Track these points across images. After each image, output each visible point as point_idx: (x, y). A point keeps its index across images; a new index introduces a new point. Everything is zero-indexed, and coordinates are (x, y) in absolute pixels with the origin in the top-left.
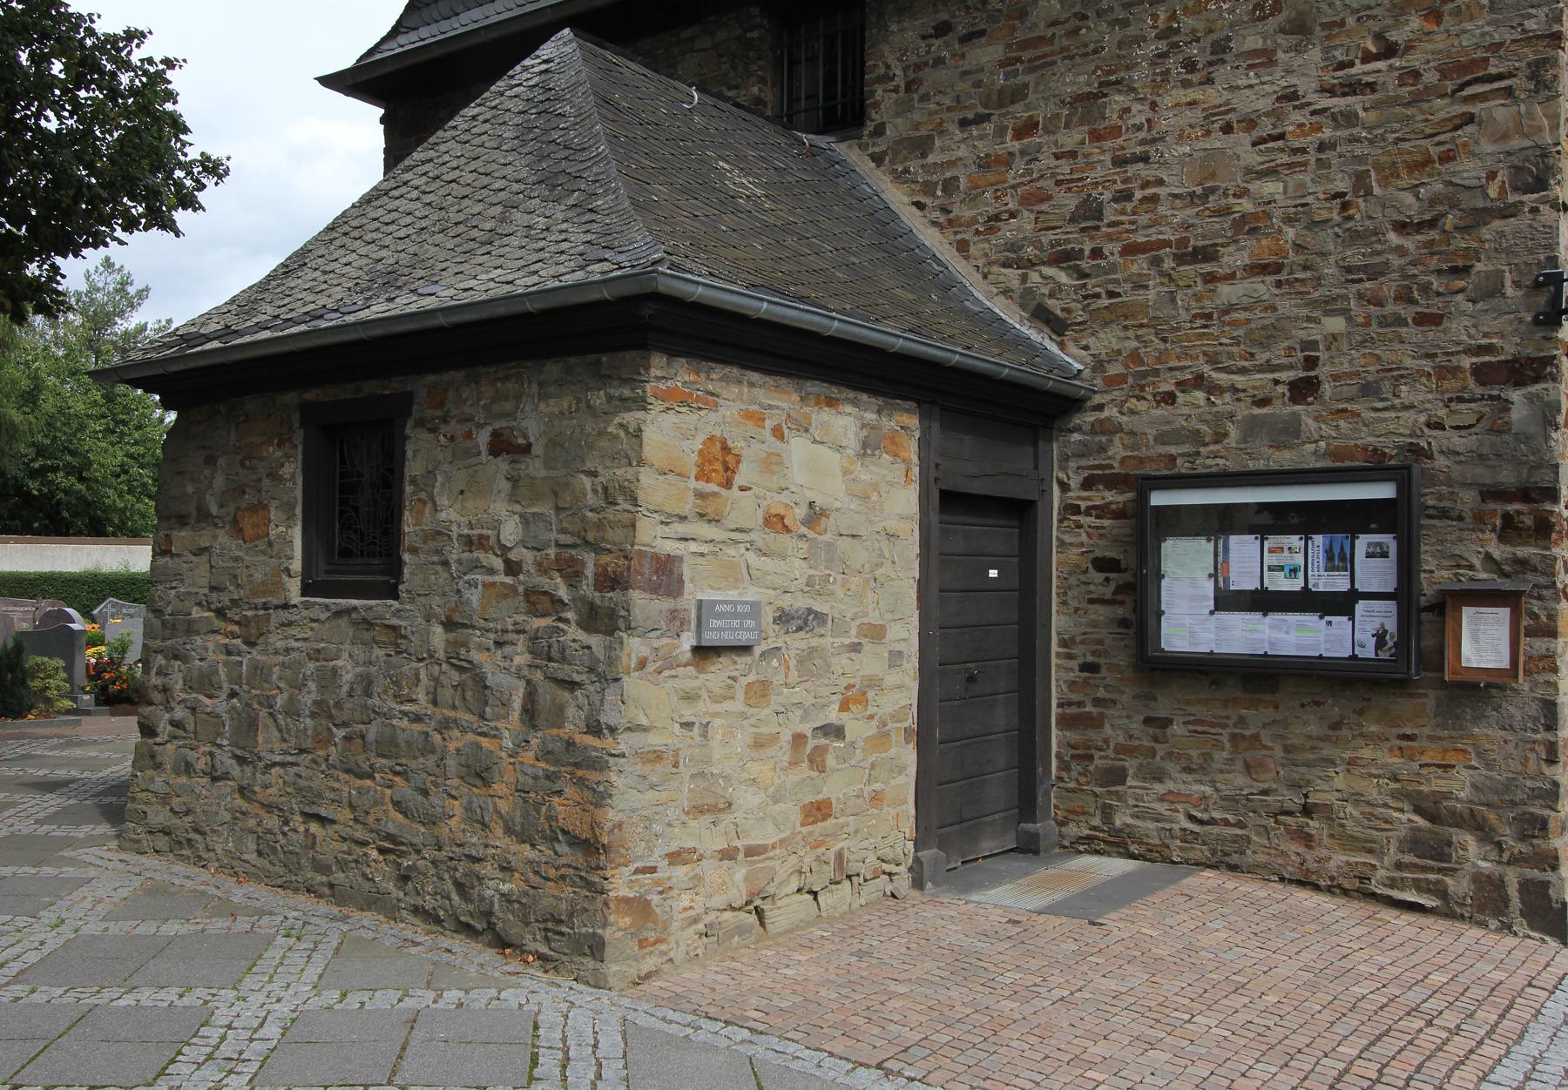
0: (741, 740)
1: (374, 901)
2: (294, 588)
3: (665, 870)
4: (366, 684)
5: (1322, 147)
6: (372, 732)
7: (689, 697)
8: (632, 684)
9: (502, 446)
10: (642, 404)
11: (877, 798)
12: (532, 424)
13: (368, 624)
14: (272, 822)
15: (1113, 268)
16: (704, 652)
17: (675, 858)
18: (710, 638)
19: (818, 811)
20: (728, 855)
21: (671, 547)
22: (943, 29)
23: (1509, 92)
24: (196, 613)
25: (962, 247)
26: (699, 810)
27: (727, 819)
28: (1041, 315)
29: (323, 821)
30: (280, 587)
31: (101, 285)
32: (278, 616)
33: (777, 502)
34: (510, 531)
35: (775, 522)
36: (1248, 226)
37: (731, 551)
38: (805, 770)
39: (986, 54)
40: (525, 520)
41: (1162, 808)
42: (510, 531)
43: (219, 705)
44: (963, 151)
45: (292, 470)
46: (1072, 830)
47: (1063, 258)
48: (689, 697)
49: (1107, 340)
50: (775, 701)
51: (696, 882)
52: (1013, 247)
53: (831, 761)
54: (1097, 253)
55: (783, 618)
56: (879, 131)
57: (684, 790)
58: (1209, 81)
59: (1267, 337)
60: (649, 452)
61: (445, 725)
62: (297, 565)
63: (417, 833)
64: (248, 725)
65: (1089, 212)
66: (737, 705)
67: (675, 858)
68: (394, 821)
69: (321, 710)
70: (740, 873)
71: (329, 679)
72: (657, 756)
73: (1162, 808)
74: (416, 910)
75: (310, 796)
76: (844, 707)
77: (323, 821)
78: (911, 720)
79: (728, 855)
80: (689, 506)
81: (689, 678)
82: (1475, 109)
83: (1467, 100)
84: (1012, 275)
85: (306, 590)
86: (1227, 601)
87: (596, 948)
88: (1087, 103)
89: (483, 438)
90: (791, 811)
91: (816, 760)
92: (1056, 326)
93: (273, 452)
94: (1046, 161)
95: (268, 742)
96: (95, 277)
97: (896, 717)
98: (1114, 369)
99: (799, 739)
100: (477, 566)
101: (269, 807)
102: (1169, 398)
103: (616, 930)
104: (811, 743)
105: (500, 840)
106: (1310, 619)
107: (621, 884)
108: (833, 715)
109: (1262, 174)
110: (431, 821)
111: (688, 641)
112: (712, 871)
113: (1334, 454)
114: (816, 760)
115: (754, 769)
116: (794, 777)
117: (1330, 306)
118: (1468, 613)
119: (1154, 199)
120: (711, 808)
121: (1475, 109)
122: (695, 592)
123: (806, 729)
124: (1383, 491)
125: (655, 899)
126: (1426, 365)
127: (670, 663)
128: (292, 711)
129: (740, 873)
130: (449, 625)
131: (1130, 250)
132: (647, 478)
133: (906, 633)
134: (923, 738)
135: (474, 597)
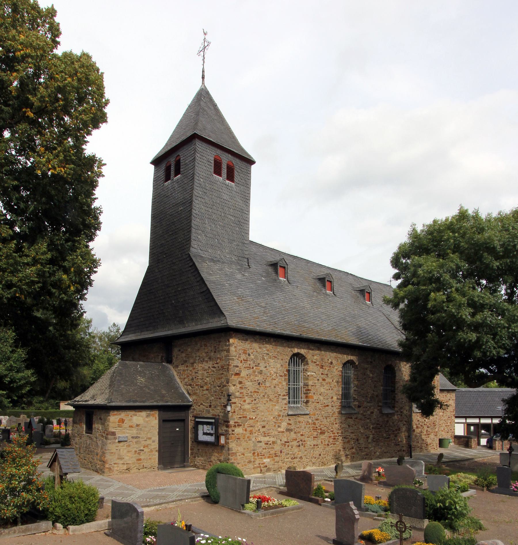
0: (125, 451)
1: (89, 469)
2: (84, 433)
3: (113, 465)
4: (89, 444)
5: (212, 375)
6: (90, 450)
7: (117, 446)
8: (109, 445)
9: (100, 419)
10: (110, 416)
11: (150, 459)
12: (102, 417)
13: (90, 437)
14: (81, 460)
15: (195, 387)
16: (119, 442)
17: (115, 464)
18: (120, 440)
19: (140, 460)
20: (123, 464)
21: (114, 431)
22: (180, 350)
23: (225, 371)
24: (76, 435)
25: (181, 382)
26: (119, 459)
27: (124, 460)
28: (188, 393)
29: (86, 460)
30: (82, 432)
31: (112, 330)
32: (83, 436)
33: (131, 424)
34: (100, 428)
35: (131, 427)
36: (206, 383)
37: (124, 430)
38: (137, 455)
39: (184, 355)
40: (102, 427)
41: (199, 461)
42: (100, 428)
43: (77, 446)
44: (181, 368)
45: (84, 418)
46: (192, 464)
47: (190, 385)
48: (117, 446)
49: (194, 397)
50: (131, 447)
51: (118, 467)
52: (186, 383)
53: (141, 454)
54: (193, 385)
55: (133, 437)
56: (173, 364)
57: (117, 456)
58: (203, 364)
59: (207, 399)
60: (111, 421)
61: (95, 449)
62: (85, 430)
63: (93, 461)
64: (80, 449)
65: (193, 379)
66: (125, 447)
67: (115, 464)
68: (91, 460)
69: (86, 447)
70: (125, 466)
71: (87, 443)
72: (112, 453)
73: (199, 461)
74: (93, 470)
75: (85, 457)
76: (144, 447)
77: (86, 460)
78: (157, 449)
79: (123, 464)
80: (117, 426)
81: (118, 444)
82: (223, 372)
83: (223, 371)
84: (186, 386)
85: (86, 433)
86: (205, 434)
87: (104, 472)
88: (193, 364)
89: (99, 417)
90: (134, 460)
91: (139, 454)
92: (190, 394)
93: (83, 416)
94: (189, 371)
95: (82, 451)
96: (111, 328)
97: (154, 449)
98: (195, 401)
99: (136, 451)
100: (98, 432)
101: (81, 458)
102: (199, 406)
103: (106, 470)
104: (138, 452)
105: (99, 462)
106: (210, 436)
107: (107, 466)
108: (142, 448)
109: (207, 377)
110: (94, 460)
111: (117, 441)
112: (121, 466)
113: (213, 415)
114: (139, 454)
115: (128, 454)
116: (135, 456)
117: (212, 396)
118: (222, 436)
119: (198, 378)
120: (121, 458)
121: (223, 372)
122: (117, 435)
123: (137, 450)
124: (213, 421)
125: (112, 468)
126: (220, 404)
127: (114, 443)
128: (83, 447)
129: (125, 466)
130: (96, 438)
131: (196, 385)
132: (110, 424)
133: (156, 438)
134: (159, 451)
135: (98, 435)
